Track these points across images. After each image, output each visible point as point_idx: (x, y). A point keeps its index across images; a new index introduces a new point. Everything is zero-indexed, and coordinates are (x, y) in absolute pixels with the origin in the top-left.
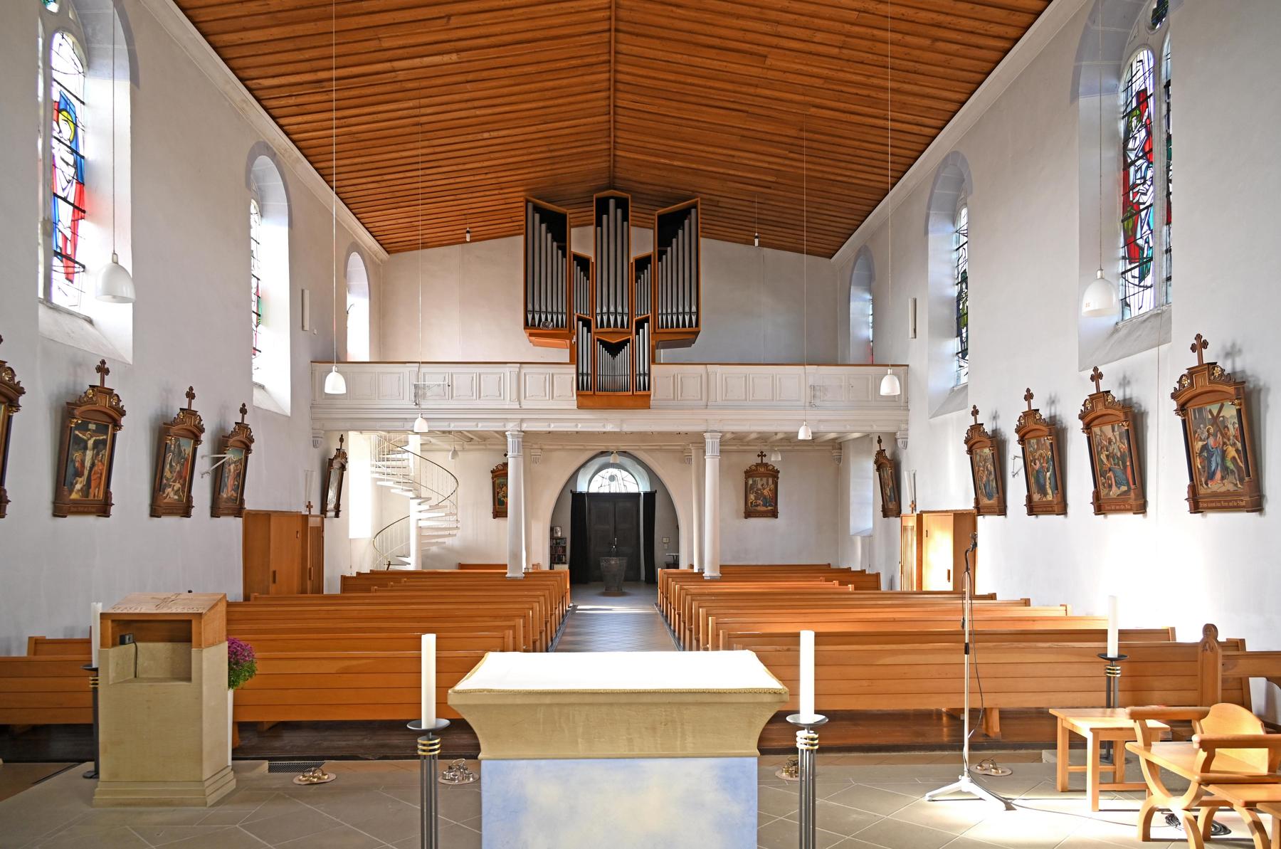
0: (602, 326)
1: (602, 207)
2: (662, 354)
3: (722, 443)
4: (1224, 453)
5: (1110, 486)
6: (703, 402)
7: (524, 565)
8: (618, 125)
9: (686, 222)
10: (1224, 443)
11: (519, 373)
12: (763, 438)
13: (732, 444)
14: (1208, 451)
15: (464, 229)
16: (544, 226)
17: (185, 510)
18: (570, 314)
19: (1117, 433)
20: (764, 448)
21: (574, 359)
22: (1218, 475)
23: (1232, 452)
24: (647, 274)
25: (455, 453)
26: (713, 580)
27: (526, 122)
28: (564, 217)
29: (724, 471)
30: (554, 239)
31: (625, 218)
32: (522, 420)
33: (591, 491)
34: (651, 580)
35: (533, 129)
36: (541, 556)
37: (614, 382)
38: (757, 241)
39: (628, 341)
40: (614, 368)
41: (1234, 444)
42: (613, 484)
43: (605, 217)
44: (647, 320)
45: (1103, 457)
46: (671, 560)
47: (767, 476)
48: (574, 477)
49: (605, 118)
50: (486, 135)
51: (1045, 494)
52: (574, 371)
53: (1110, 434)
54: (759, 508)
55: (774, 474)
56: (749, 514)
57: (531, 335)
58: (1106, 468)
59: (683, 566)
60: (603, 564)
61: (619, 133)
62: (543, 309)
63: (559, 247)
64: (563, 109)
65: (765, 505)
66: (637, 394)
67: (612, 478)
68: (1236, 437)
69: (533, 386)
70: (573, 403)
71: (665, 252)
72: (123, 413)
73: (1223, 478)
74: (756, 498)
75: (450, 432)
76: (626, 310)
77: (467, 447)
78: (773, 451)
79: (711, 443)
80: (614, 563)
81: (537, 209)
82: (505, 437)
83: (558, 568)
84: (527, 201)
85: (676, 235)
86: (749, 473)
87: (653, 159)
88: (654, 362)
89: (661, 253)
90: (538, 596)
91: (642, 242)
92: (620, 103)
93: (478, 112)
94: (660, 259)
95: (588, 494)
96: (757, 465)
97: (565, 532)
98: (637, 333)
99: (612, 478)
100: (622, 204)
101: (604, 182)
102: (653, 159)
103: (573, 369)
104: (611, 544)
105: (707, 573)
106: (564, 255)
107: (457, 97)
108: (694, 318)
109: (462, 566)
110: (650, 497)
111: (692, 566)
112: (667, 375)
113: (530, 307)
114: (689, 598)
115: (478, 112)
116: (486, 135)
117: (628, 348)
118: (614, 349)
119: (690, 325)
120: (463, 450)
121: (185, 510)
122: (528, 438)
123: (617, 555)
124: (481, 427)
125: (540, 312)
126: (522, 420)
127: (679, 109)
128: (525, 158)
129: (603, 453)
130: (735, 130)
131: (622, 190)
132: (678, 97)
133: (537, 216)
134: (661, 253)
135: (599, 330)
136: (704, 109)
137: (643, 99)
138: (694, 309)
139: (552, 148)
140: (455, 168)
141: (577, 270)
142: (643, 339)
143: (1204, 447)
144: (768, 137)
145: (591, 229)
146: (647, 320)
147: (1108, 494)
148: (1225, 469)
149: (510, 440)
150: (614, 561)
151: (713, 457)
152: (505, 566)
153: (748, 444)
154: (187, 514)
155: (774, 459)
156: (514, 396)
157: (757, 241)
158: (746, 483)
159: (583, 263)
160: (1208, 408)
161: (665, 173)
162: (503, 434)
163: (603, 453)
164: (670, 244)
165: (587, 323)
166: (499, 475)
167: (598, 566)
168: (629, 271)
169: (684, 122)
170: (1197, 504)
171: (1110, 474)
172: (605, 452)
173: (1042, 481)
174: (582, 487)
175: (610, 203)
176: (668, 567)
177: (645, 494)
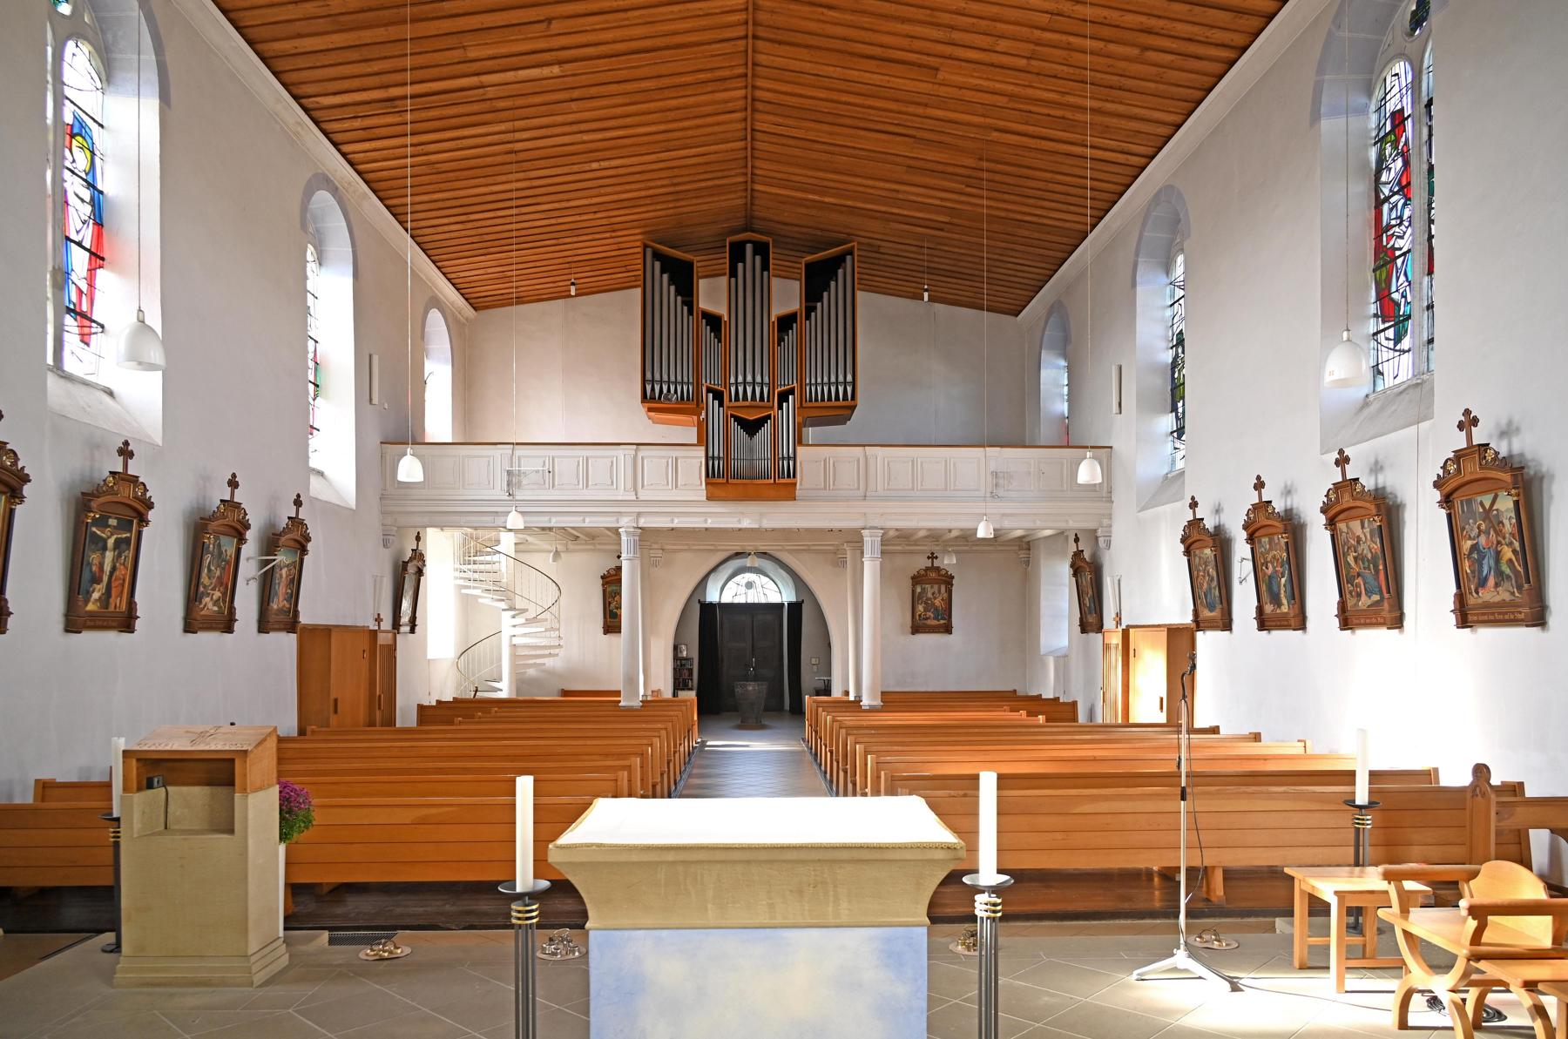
0: (737, 399)
1: (737, 253)
2: (811, 433)
3: (883, 543)
4: (1498, 554)
5: (1359, 595)
6: (861, 492)
7: (642, 692)
8: (757, 154)
9: (840, 271)
10: (1499, 543)
11: (635, 456)
12: (935, 536)
13: (896, 543)
14: (1479, 552)
16: (665, 277)
17: (226, 624)
18: (698, 385)
19: (1367, 530)
20: (935, 549)
21: (703, 439)
22: (1491, 582)
23: (1508, 554)
24: (792, 335)
25: (557, 554)
26: (872, 710)
28: (690, 265)
29: (886, 576)
30: (678, 292)
31: (765, 267)
32: (639, 514)
33: (724, 600)
34: (797, 710)
35: (653, 157)
36: (662, 681)
37: (752, 467)
38: (926, 295)
39: (769, 417)
40: (751, 450)
41: (1511, 544)
42: (751, 592)
43: (740, 265)
44: (792, 391)
45: (1350, 559)
46: (821, 685)
47: (938, 582)
48: (702, 584)
49: (741, 144)
50: (595, 165)
51: (1279, 605)
52: (703, 454)
53: (1359, 532)
54: (929, 622)
55: (948, 580)
56: (916, 629)
57: (650, 410)
58: (1353, 573)
59: (837, 693)
60: (738, 690)
61: (758, 163)
63: (684, 303)
64: (690, 133)
65: (936, 618)
66: (780, 482)
67: (749, 585)
68: (1512, 535)
69: (652, 473)
70: (701, 493)
71: (814, 309)
73: (1497, 585)
74: (926, 610)
75: (550, 529)
76: (766, 380)
77: (571, 547)
78: (946, 552)
79: (871, 542)
80: (752, 689)
81: (657, 255)
82: (619, 534)
83: (683, 695)
84: (645, 246)
85: (827, 288)
86: (917, 579)
87: (799, 195)
88: (800, 443)
89: (810, 310)
90: (658, 730)
91: (786, 296)
92: (758, 126)
93: (585, 137)
94: (808, 317)
95: (720, 604)
96: (927, 569)
97: (691, 651)
98: (780, 407)
99: (749, 585)
100: (761, 250)
101: (740, 223)
102: (799, 195)
103: (701, 452)
104: (748, 666)
105: (866, 702)
106: (690, 312)
107: (559, 119)
108: (849, 389)
109: (565, 693)
110: (795, 608)
111: (847, 693)
112: (817, 459)
113: (649, 376)
114: (843, 731)
115: (585, 137)
116: (595, 165)
117: (768, 426)
118: (752, 427)
119: (845, 398)
120: (567, 550)
121: (226, 624)
122: (646, 536)
123: (755, 679)
124: (589, 522)
125: (661, 382)
126: (639, 514)
127: (831, 134)
128: (643, 193)
129: (738, 555)
130: (899, 160)
131: (761, 233)
132: (830, 119)
133: (658, 265)
134: (810, 310)
135: (733, 403)
136: (862, 133)
137: (787, 121)
138: (849, 378)
139: (675, 181)
140: (556, 205)
141: (706, 330)
142: (787, 414)
143: (1474, 548)
144: (941, 168)
145: (724, 280)
146: (792, 391)
147: (1356, 605)
148: (1500, 574)
149: (624, 538)
150: (751, 687)
151: (873, 559)
152: (618, 693)
153: (916, 543)
154: (228, 629)
155: (948, 562)
156: (630, 485)
157: (926, 295)
158: (913, 592)
159: (714, 321)
160: (1479, 499)
161: (813, 212)
162: (616, 531)
163: (738, 555)
164: (820, 299)
165: (718, 396)
166: (611, 581)
167: (732, 693)
168: (770, 332)
169: (837, 149)
170: (1465, 616)
171: (1359, 580)
172: (740, 553)
173: (1275, 588)
174: (712, 596)
175: (747, 249)
176: (818, 693)
177: (790, 604)
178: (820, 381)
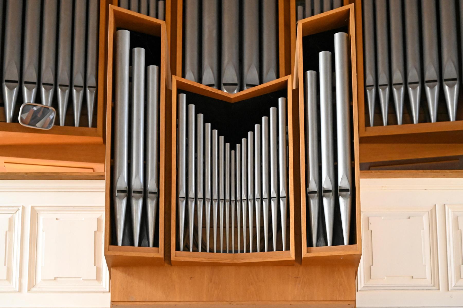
37: (235, 222)
40: (233, 176)
98: (311, 63)
118: (234, 120)
165: (147, 39)
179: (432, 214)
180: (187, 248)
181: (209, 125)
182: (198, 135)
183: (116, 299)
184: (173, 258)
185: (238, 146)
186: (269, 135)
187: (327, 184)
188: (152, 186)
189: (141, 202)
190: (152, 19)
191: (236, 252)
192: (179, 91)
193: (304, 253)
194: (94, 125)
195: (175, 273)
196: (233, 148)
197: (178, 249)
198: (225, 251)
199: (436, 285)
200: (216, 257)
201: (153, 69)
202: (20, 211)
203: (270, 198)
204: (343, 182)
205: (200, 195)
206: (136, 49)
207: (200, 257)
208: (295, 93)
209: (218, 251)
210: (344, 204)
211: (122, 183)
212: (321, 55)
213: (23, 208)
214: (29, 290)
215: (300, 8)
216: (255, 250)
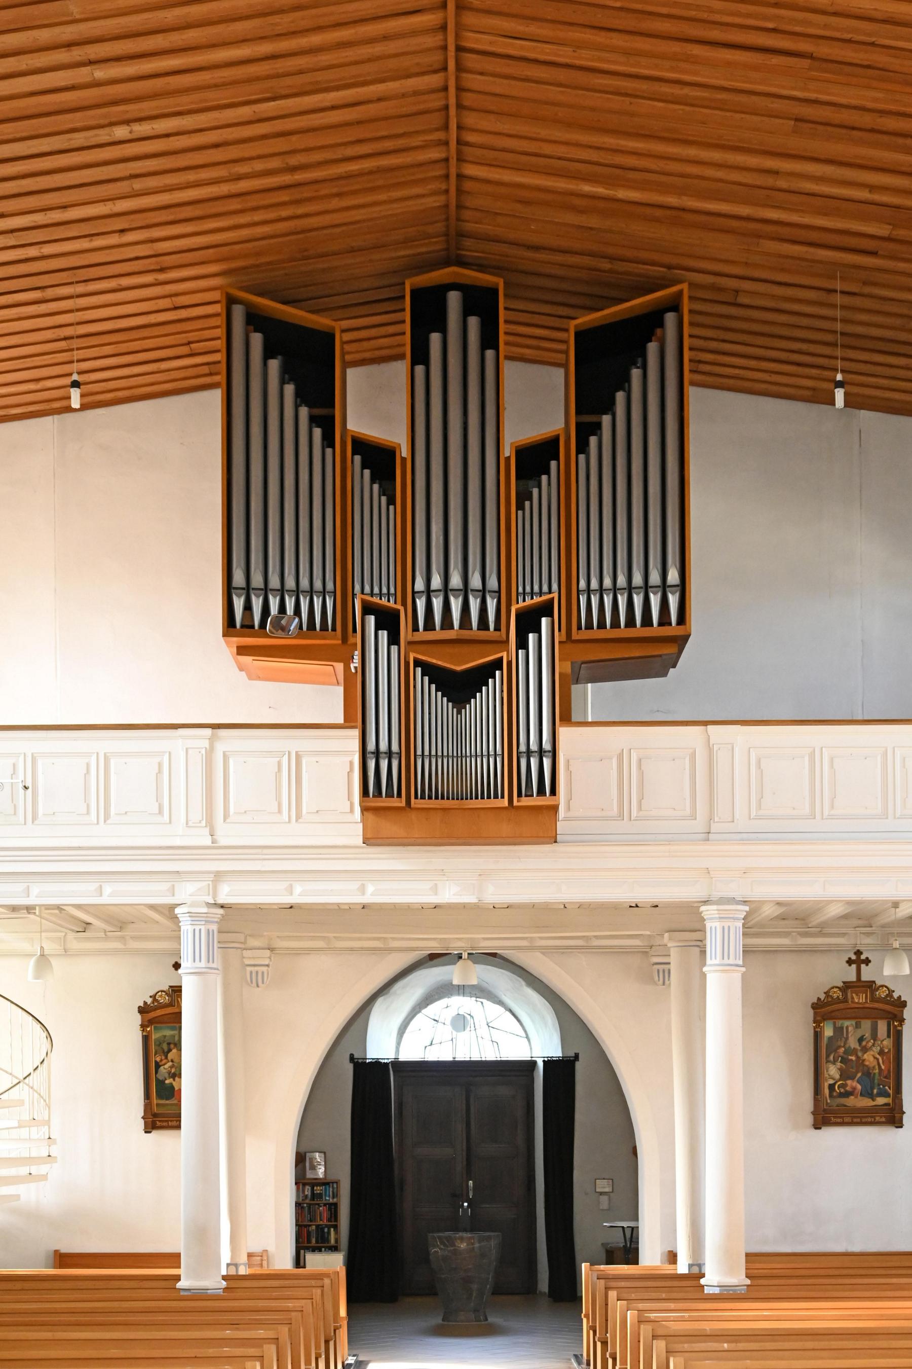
0: (429, 624)
1: (428, 312)
2: (592, 696)
3: (750, 928)
6: (699, 825)
7: (226, 1257)
8: (469, 99)
9: (652, 348)
11: (210, 752)
12: (862, 916)
13: (777, 933)
15: (113, 374)
16: (274, 365)
18: (345, 597)
20: (865, 942)
21: (357, 713)
24: (547, 488)
25: (43, 960)
26: (727, 1296)
27: (214, 97)
28: (327, 339)
29: (755, 1002)
30: (301, 398)
31: (489, 340)
32: (218, 876)
33: (403, 1057)
34: (565, 1292)
35: (245, 112)
36: (266, 1226)
37: (461, 773)
38: (839, 394)
39: (498, 664)
40: (459, 736)
42: (463, 1037)
43: (435, 338)
44: (546, 609)
46: (618, 1240)
47: (873, 1014)
48: (358, 1020)
49: (435, 80)
50: (121, 132)
52: (355, 745)
54: (851, 1101)
55: (891, 1011)
56: (825, 1116)
57: (242, 650)
59: (650, 1256)
60: (437, 1251)
61: (470, 119)
62: (290, 583)
63: (314, 420)
64: (325, 59)
65: (868, 1093)
66: (523, 801)
67: (460, 1022)
69: (249, 781)
70: (352, 826)
71: (596, 428)
72: (904, 1004)
74: (845, 1075)
75: (29, 909)
76: (492, 583)
77: (75, 943)
78: (886, 948)
79: (722, 934)
80: (466, 1250)
81: (255, 320)
82: (175, 919)
83: (317, 1262)
84: (231, 301)
85: (623, 382)
86: (824, 1009)
87: (562, 184)
88: (567, 719)
89: (586, 431)
90: (257, 1342)
91: (535, 401)
92: (472, 40)
93: (100, 73)
94: (582, 447)
95: (398, 1065)
96: (847, 986)
97: (335, 1165)
98: (522, 644)
99: (460, 1022)
100: (480, 303)
101: (435, 246)
102: (562, 184)
103: (351, 740)
104: (458, 1196)
105: (714, 1277)
106: (328, 440)
107: (44, 36)
108: (673, 601)
109: (63, 1259)
110: (561, 1072)
111: (672, 1257)
112: (605, 752)
113: (239, 578)
114: (660, 1346)
115: (100, 73)
116: (121, 132)
117: (496, 683)
118: (460, 687)
119: (664, 620)
120: (66, 952)
122: (236, 925)
123: (475, 1225)
124: (113, 894)
125: (266, 591)
126: (218, 876)
127: (627, 53)
128: (224, 189)
129: (433, 958)
130: (777, 105)
131: (481, 267)
132: (630, 22)
133: (257, 339)
134: (586, 431)
135: (422, 635)
136: (697, 50)
137: (532, 29)
138: (673, 576)
139: (294, 161)
140: (39, 218)
141: (362, 478)
142: (536, 661)
144: (867, 120)
145: (401, 368)
146: (546, 609)
149: (186, 927)
150: (463, 1243)
151: (726, 968)
152: (174, 1259)
153: (822, 930)
155: (891, 971)
156: (197, 813)
157: (839, 394)
158: (817, 1036)
159: (378, 459)
161: (593, 221)
162: (170, 912)
163: (433, 958)
164: (609, 408)
165: (388, 621)
166: (160, 1019)
167: (425, 1259)
168: (501, 480)
169: (644, 86)
172: (434, 958)
174: (381, 1046)
175: (450, 302)
176: (611, 1259)
177: (548, 1063)
178: (604, 592)
179: (620, 757)
180: (423, 797)
181: (439, 694)
182: (431, 701)
183: (369, 836)
184: (413, 805)
185: (463, 711)
186: (488, 700)
187: (534, 747)
188: (395, 748)
189: (386, 761)
190: (391, 604)
191: (462, 799)
192: (415, 666)
193: (515, 803)
194: (334, 629)
195: (413, 815)
196: (459, 712)
197: (416, 798)
198: (453, 799)
199: (621, 816)
200: (446, 803)
201: (394, 648)
202: (287, 756)
203: (489, 755)
204: (547, 746)
205: (433, 753)
206: (380, 632)
207: (433, 803)
208: (509, 663)
209: (448, 799)
210: (547, 762)
211: (371, 746)
212: (531, 636)
213: (289, 752)
214: (297, 821)
215: (520, 512)
216: (477, 798)
